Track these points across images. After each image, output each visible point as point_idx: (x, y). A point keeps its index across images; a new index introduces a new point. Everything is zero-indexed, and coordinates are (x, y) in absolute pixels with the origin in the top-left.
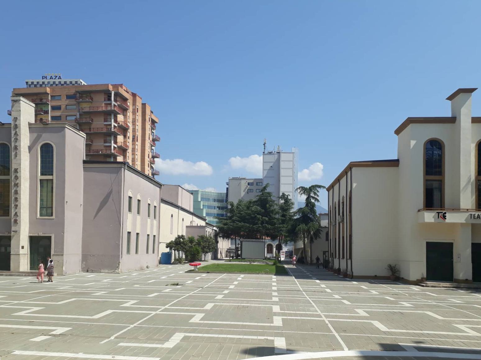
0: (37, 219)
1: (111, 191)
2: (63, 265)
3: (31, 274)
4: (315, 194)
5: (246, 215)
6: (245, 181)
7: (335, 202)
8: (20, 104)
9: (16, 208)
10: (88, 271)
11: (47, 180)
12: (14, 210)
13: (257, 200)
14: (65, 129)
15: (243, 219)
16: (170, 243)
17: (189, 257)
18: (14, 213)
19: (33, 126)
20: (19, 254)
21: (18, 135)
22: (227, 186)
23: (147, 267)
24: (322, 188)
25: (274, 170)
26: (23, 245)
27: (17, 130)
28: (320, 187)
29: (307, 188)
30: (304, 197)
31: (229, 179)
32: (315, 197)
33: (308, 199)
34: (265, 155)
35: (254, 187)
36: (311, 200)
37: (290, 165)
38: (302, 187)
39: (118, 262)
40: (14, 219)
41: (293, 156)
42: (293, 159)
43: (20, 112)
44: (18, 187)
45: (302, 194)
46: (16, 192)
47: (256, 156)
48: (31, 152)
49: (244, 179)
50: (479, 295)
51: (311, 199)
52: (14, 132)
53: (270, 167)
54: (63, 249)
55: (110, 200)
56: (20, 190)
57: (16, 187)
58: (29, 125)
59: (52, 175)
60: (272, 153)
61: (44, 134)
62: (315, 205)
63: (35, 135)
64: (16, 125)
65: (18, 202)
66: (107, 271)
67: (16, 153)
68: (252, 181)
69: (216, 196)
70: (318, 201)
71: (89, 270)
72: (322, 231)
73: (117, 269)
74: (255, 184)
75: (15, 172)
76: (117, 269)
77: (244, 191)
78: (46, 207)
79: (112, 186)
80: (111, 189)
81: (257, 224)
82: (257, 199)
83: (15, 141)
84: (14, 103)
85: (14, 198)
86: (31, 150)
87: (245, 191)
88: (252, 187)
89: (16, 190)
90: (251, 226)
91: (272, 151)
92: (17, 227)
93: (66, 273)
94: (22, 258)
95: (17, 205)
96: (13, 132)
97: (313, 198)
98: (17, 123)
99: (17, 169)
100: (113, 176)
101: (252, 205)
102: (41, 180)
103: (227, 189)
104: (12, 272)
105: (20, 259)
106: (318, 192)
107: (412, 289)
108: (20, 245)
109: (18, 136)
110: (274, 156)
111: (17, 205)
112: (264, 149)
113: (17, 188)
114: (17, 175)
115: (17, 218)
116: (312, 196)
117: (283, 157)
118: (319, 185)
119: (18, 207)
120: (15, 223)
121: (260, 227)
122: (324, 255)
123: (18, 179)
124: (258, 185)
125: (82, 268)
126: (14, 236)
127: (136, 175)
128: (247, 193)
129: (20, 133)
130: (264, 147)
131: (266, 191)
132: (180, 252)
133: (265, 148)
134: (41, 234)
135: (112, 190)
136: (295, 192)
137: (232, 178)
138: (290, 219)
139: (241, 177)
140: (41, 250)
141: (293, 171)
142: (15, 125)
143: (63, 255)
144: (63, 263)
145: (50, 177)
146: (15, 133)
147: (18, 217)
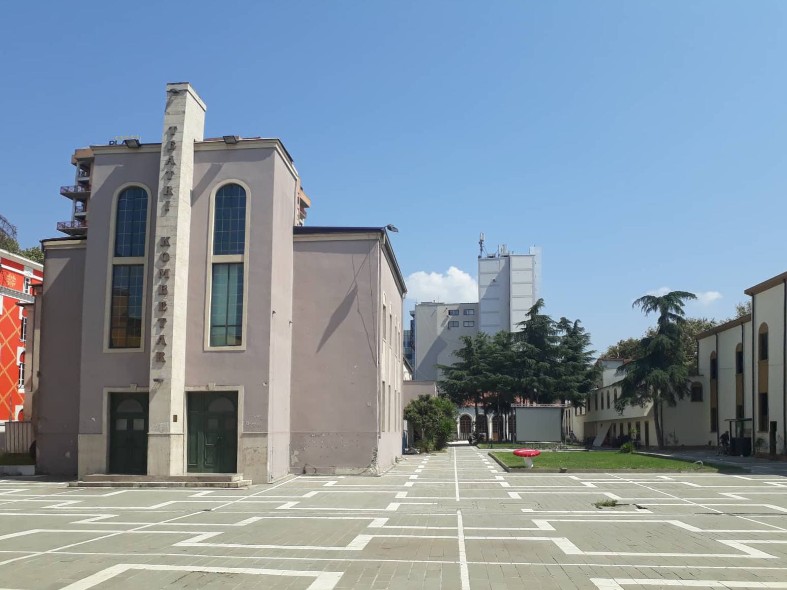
0: (204, 352)
1: (353, 291)
2: (266, 459)
3: (190, 483)
4: (677, 309)
6: (443, 308)
8: (185, 98)
9: (162, 327)
10: (304, 472)
11: (229, 265)
12: (157, 330)
13: (522, 331)
14: (272, 152)
15: (497, 367)
17: (434, 438)
18: (158, 338)
19: (202, 148)
20: (169, 435)
21: (174, 164)
22: (412, 319)
24: (689, 297)
25: (500, 288)
26: (176, 414)
27: (174, 153)
28: (685, 295)
30: (657, 314)
31: (416, 306)
33: (662, 320)
34: (482, 260)
35: (460, 318)
36: (668, 321)
37: (527, 277)
38: (649, 297)
39: (372, 450)
40: (157, 351)
41: (533, 261)
42: (533, 266)
43: (184, 116)
44: (167, 278)
45: (648, 310)
46: (163, 291)
47: (423, 273)
48: (196, 203)
49: (442, 304)
50: (734, 496)
52: (167, 158)
53: (492, 281)
54: (265, 421)
55: (353, 311)
56: (173, 286)
57: (163, 278)
58: (195, 146)
59: (242, 253)
60: (495, 257)
61: (225, 164)
63: (207, 166)
64: (173, 143)
65: (166, 313)
66: (348, 471)
67: (168, 203)
68: (456, 308)
71: (307, 468)
73: (372, 465)
74: (461, 313)
75: (161, 246)
76: (372, 465)
77: (442, 325)
78: (225, 324)
79: (355, 280)
80: (354, 285)
81: (527, 375)
82: (522, 329)
83: (166, 177)
84: (173, 98)
85: (157, 303)
86: (195, 201)
87: (445, 326)
88: (456, 318)
89: (163, 287)
90: (516, 379)
91: (495, 254)
92: (163, 369)
93: (272, 478)
94: (171, 444)
95: (164, 320)
96: (164, 159)
97: (673, 316)
98: (174, 139)
99: (168, 238)
100: (359, 258)
101: (512, 340)
102: (214, 265)
103: (412, 323)
104: (153, 478)
105: (172, 445)
106: (682, 305)
107: (724, 496)
108: (171, 414)
109: (175, 167)
110: (498, 262)
111: (164, 320)
112: (480, 251)
113: (165, 283)
114: (168, 252)
115: (163, 348)
116: (671, 314)
117: (515, 263)
118: (683, 293)
119: (166, 325)
120: (157, 361)
123: (168, 260)
124: (466, 315)
125: (291, 465)
126: (155, 392)
127: (388, 265)
128: (448, 328)
129: (180, 160)
130: (480, 248)
133: (481, 250)
134: (214, 387)
135: (356, 287)
136: (633, 306)
137: (420, 304)
139: (436, 302)
140: (213, 423)
141: (533, 287)
142: (170, 144)
143: (265, 435)
144: (267, 454)
145: (236, 258)
146: (170, 159)
147: (166, 348)
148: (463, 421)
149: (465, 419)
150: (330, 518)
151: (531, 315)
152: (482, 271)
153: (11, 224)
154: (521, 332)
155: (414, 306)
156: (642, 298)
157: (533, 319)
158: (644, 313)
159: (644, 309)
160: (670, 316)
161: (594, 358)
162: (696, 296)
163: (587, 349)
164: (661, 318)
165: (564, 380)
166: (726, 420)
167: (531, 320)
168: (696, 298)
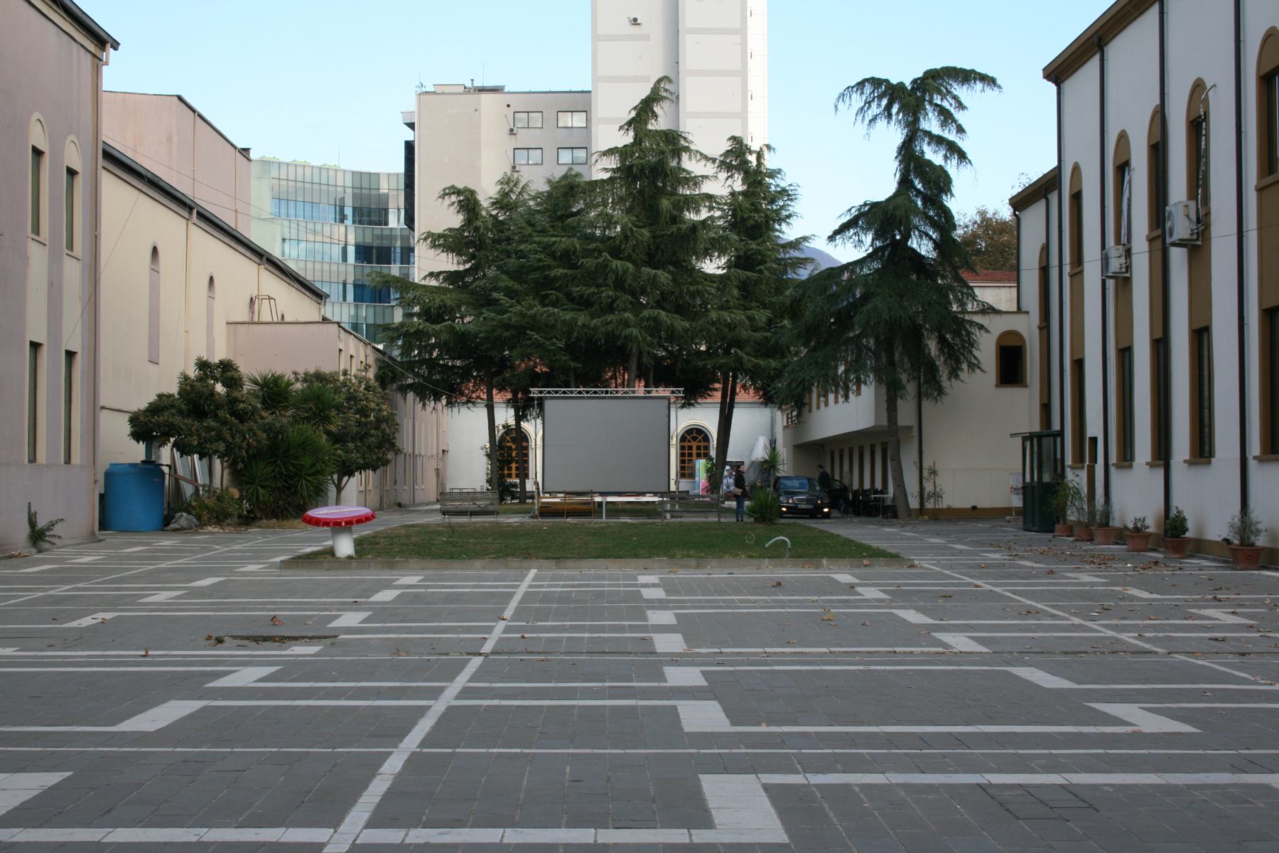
4: (946, 117)
5: (549, 261)
7: (1123, 137)
13: (606, 176)
16: (154, 409)
22: (409, 135)
23: (38, 536)
28: (966, 76)
29: (901, 85)
30: (892, 134)
32: (946, 135)
33: (909, 156)
45: (874, 120)
51: (926, 148)
62: (948, 180)
69: (349, 191)
70: (962, 156)
72: (981, 327)
82: (606, 170)
97: (939, 141)
103: (409, 147)
106: (961, 106)
121: (627, 324)
122: (1059, 456)
131: (652, 126)
132: (217, 463)
138: (781, 285)
148: (686, 444)
149: (695, 439)
150: (873, 668)
151: (635, 130)
152: (737, 38)
153: (979, 85)
154: (602, 180)
155: (414, 99)
156: (859, 84)
157: (638, 140)
158: (862, 127)
159: (860, 118)
160: (927, 140)
161: (806, 259)
162: (999, 82)
163: (788, 232)
164: (904, 143)
165: (713, 323)
166: (1013, 435)
167: (633, 145)
168: (999, 87)
